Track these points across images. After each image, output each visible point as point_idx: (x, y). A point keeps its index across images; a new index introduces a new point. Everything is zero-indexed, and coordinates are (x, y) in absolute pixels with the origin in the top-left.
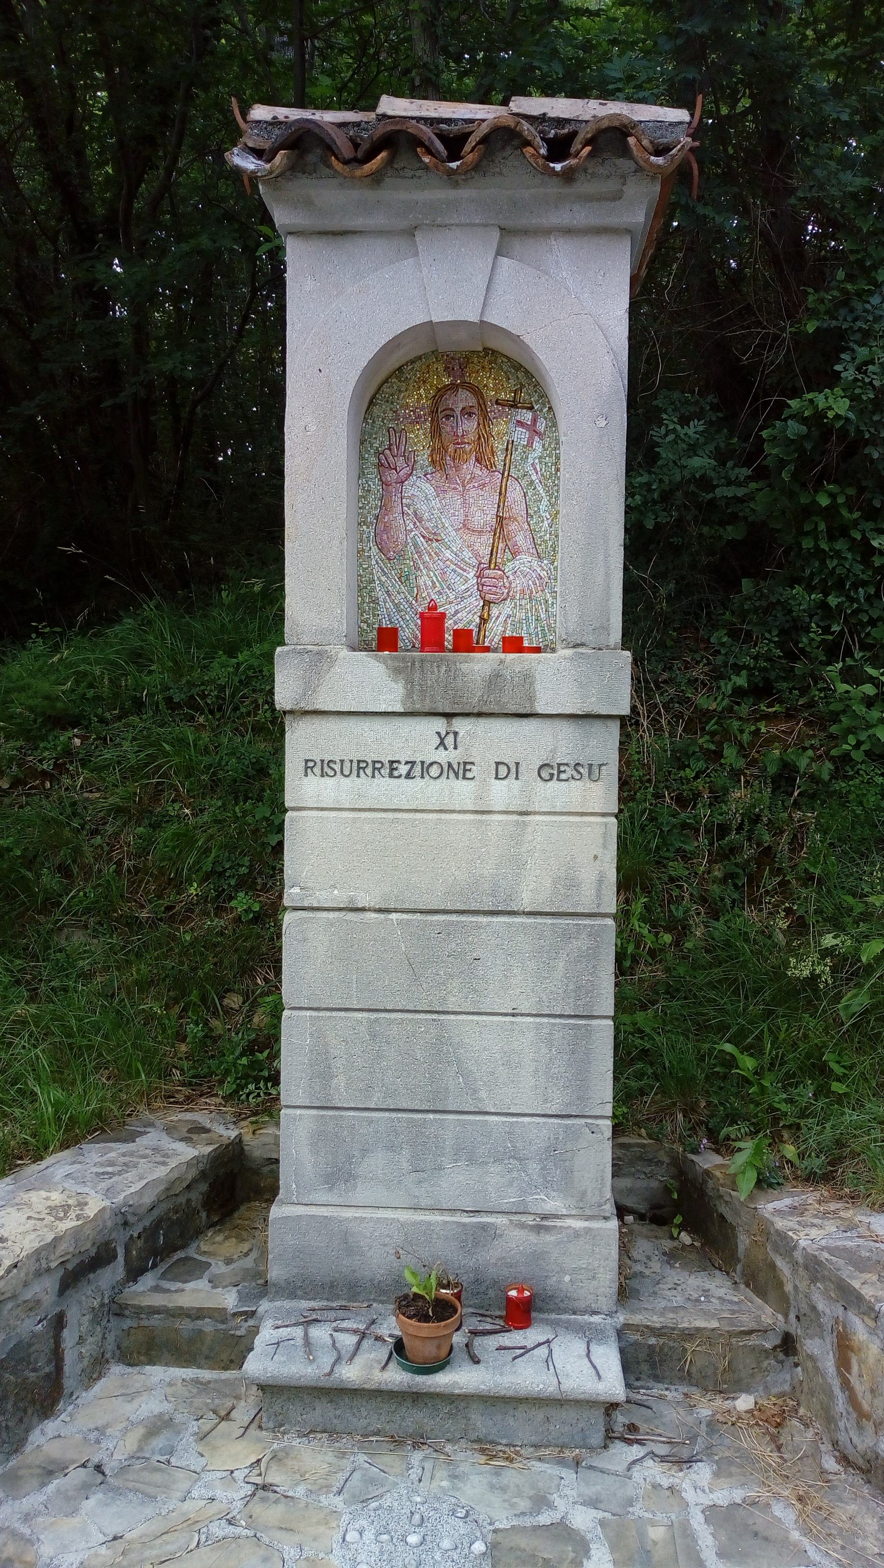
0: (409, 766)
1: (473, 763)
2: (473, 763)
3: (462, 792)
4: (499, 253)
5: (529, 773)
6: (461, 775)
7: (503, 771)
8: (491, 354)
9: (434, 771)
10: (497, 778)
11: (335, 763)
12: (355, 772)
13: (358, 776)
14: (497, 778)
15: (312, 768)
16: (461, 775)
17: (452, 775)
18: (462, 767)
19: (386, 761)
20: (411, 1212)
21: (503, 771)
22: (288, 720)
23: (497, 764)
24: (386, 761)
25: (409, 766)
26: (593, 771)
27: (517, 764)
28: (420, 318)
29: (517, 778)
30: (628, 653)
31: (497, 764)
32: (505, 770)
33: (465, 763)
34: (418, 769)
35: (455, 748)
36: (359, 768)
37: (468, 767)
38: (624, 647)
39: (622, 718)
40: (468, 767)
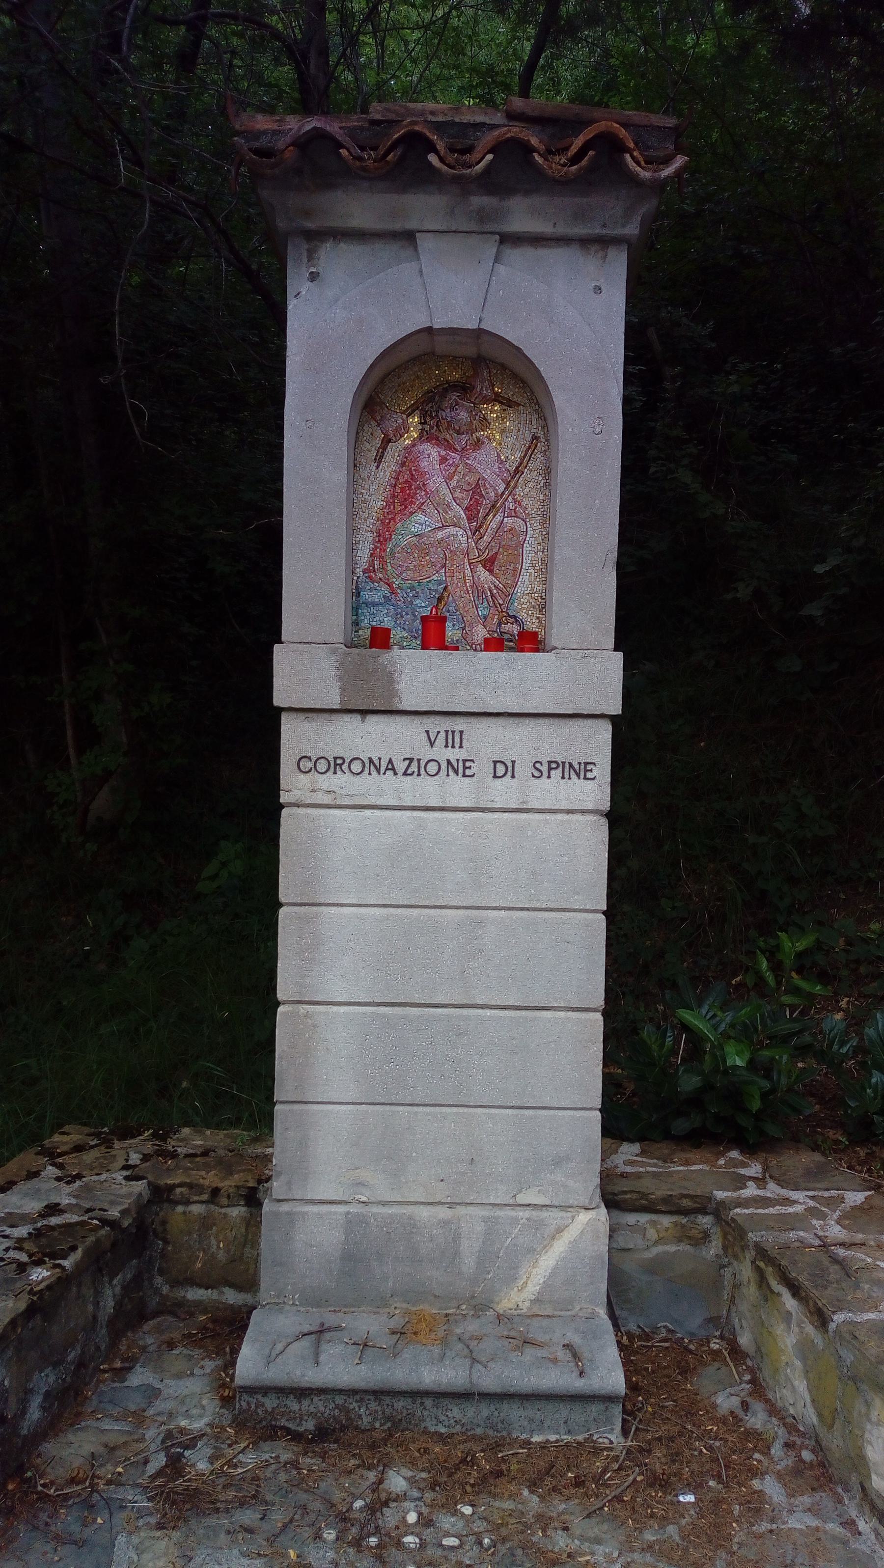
0: (407, 762)
1: (472, 761)
2: (472, 761)
3: (458, 790)
4: (497, 259)
5: (524, 769)
6: (582, 776)
7: (501, 770)
8: (479, 362)
9: (432, 768)
10: (495, 776)
11: (541, 763)
12: (332, 769)
13: (335, 773)
14: (495, 776)
15: (341, 765)
16: (582, 776)
17: (451, 773)
18: (582, 767)
19: (545, 761)
20: (380, 1207)
21: (501, 770)
22: (284, 717)
23: (495, 762)
24: (545, 761)
25: (407, 762)
26: (583, 770)
27: (513, 762)
28: (422, 322)
29: (513, 776)
30: (620, 655)
31: (495, 762)
32: (503, 769)
33: (586, 764)
34: (414, 768)
35: (461, 747)
36: (336, 765)
37: (468, 764)
38: (616, 649)
39: (613, 719)
40: (468, 764)
